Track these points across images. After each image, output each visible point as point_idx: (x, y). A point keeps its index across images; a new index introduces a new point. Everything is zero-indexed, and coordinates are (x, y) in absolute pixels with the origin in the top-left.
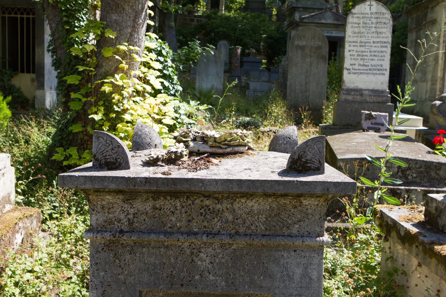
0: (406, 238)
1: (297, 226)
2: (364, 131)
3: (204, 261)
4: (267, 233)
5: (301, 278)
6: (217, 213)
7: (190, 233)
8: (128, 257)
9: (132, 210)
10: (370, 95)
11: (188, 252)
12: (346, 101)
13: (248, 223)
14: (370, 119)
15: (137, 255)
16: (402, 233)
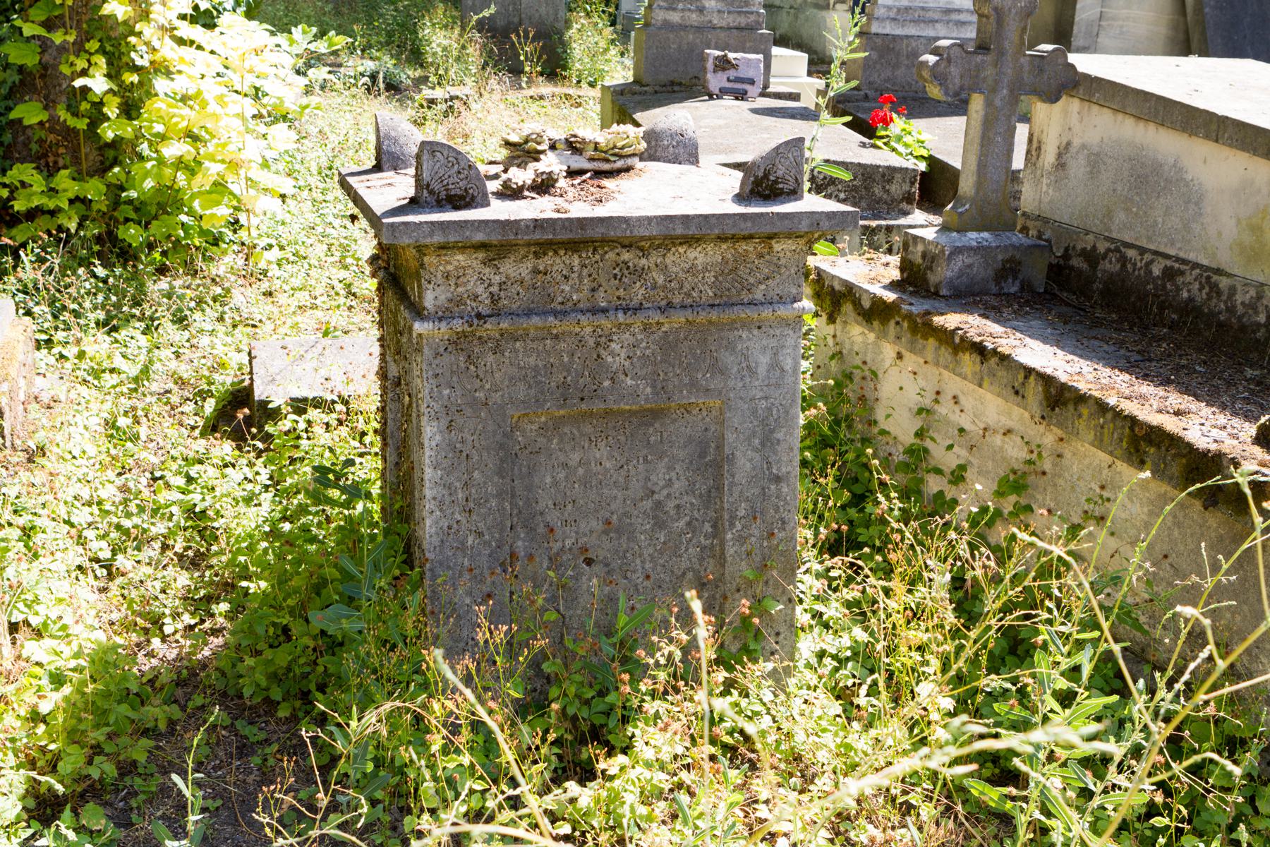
0: (876, 313)
1: (763, 287)
2: (711, 97)
3: (617, 354)
4: (717, 302)
5: (768, 371)
6: (640, 273)
7: (595, 311)
8: (490, 358)
9: (497, 277)
10: (719, 11)
11: (591, 342)
12: (667, 25)
13: (687, 287)
14: (724, 69)
15: (507, 354)
16: (866, 304)
